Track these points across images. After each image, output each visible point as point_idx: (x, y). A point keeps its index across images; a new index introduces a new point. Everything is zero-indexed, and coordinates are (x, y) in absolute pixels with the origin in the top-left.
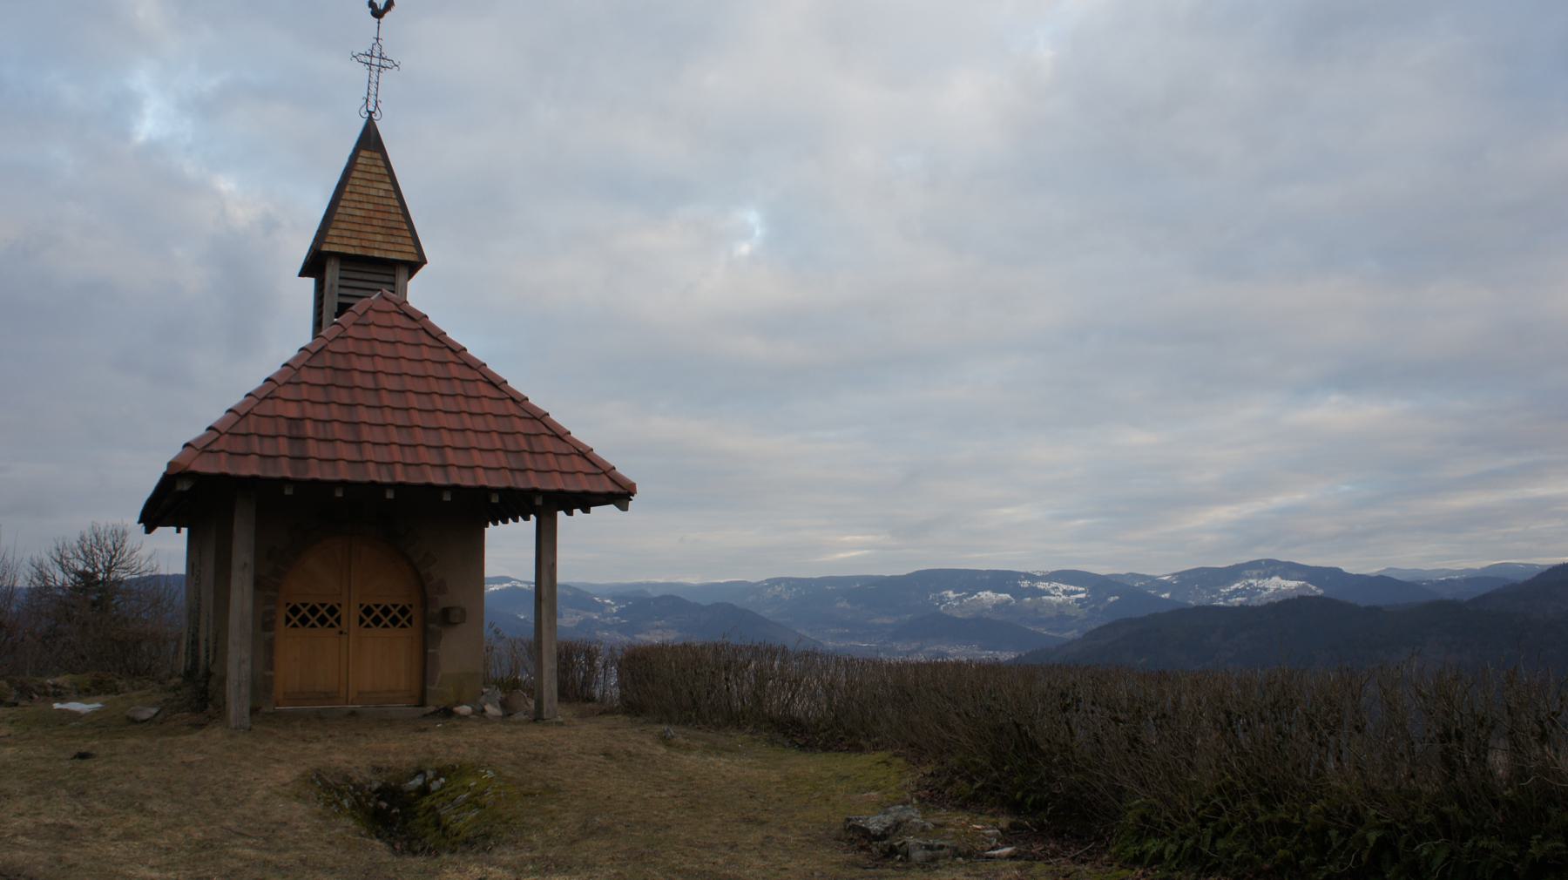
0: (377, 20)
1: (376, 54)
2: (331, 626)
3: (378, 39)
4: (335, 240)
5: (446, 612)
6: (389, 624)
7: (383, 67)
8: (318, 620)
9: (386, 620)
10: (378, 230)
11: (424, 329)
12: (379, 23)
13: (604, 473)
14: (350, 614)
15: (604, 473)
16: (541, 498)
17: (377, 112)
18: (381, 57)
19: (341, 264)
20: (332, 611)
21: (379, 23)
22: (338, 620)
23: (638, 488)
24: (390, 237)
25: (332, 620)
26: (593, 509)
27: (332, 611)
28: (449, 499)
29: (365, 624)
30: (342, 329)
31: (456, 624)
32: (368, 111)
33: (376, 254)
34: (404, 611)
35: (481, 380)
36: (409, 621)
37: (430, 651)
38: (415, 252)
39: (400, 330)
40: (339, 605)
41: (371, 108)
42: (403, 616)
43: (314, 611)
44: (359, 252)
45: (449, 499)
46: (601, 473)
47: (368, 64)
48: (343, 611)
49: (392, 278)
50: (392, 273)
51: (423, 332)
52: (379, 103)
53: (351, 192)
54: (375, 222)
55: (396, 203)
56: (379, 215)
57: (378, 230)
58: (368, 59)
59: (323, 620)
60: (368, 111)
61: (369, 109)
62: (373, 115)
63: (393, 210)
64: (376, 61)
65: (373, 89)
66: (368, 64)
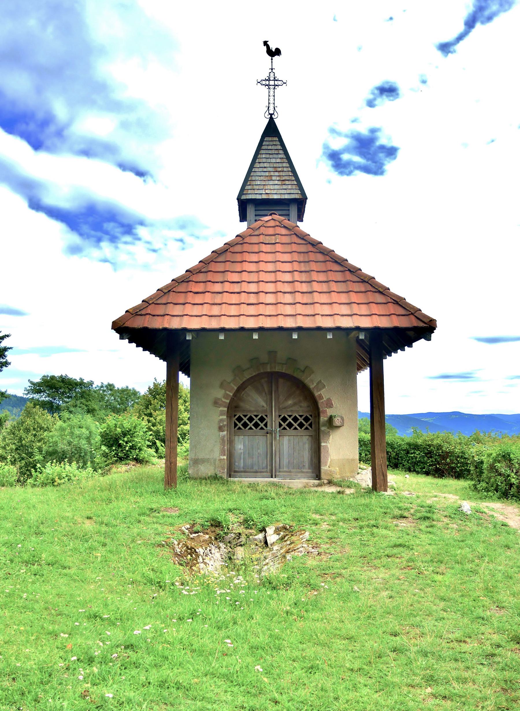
0: (271, 58)
1: (272, 79)
2: (262, 428)
3: (272, 69)
4: (250, 192)
5: (331, 419)
6: (241, 427)
7: (276, 85)
8: (253, 425)
9: (251, 425)
10: (276, 182)
11: (295, 234)
12: (272, 59)
13: (412, 314)
14: (273, 421)
15: (412, 314)
16: (363, 333)
17: (275, 113)
18: (275, 80)
19: (255, 207)
20: (262, 419)
21: (272, 59)
22: (266, 425)
23: (439, 324)
24: (284, 186)
25: (262, 425)
26: (414, 344)
27: (262, 419)
28: (296, 337)
29: (237, 427)
30: (242, 239)
31: (338, 427)
32: (269, 114)
33: (275, 197)
34: (306, 419)
35: (329, 261)
36: (310, 425)
37: (323, 444)
38: (300, 192)
39: (279, 236)
40: (266, 416)
41: (271, 112)
42: (243, 419)
43: (251, 419)
44: (264, 197)
45: (296, 337)
46: (410, 314)
47: (267, 85)
48: (268, 420)
49: (287, 211)
50: (288, 209)
51: (295, 236)
52: (276, 108)
53: (259, 163)
54: (274, 178)
55: (288, 165)
56: (277, 174)
57: (276, 182)
58: (267, 83)
59: (256, 425)
60: (269, 114)
61: (270, 112)
62: (273, 116)
63: (285, 169)
64: (272, 83)
65: (272, 101)
66: (267, 85)
